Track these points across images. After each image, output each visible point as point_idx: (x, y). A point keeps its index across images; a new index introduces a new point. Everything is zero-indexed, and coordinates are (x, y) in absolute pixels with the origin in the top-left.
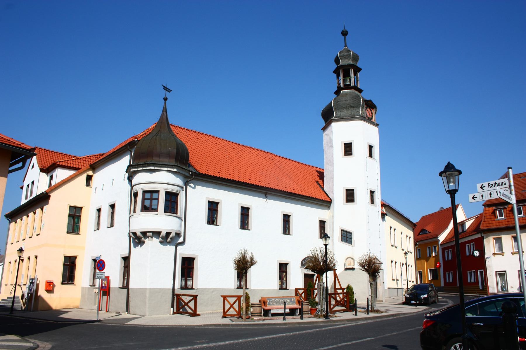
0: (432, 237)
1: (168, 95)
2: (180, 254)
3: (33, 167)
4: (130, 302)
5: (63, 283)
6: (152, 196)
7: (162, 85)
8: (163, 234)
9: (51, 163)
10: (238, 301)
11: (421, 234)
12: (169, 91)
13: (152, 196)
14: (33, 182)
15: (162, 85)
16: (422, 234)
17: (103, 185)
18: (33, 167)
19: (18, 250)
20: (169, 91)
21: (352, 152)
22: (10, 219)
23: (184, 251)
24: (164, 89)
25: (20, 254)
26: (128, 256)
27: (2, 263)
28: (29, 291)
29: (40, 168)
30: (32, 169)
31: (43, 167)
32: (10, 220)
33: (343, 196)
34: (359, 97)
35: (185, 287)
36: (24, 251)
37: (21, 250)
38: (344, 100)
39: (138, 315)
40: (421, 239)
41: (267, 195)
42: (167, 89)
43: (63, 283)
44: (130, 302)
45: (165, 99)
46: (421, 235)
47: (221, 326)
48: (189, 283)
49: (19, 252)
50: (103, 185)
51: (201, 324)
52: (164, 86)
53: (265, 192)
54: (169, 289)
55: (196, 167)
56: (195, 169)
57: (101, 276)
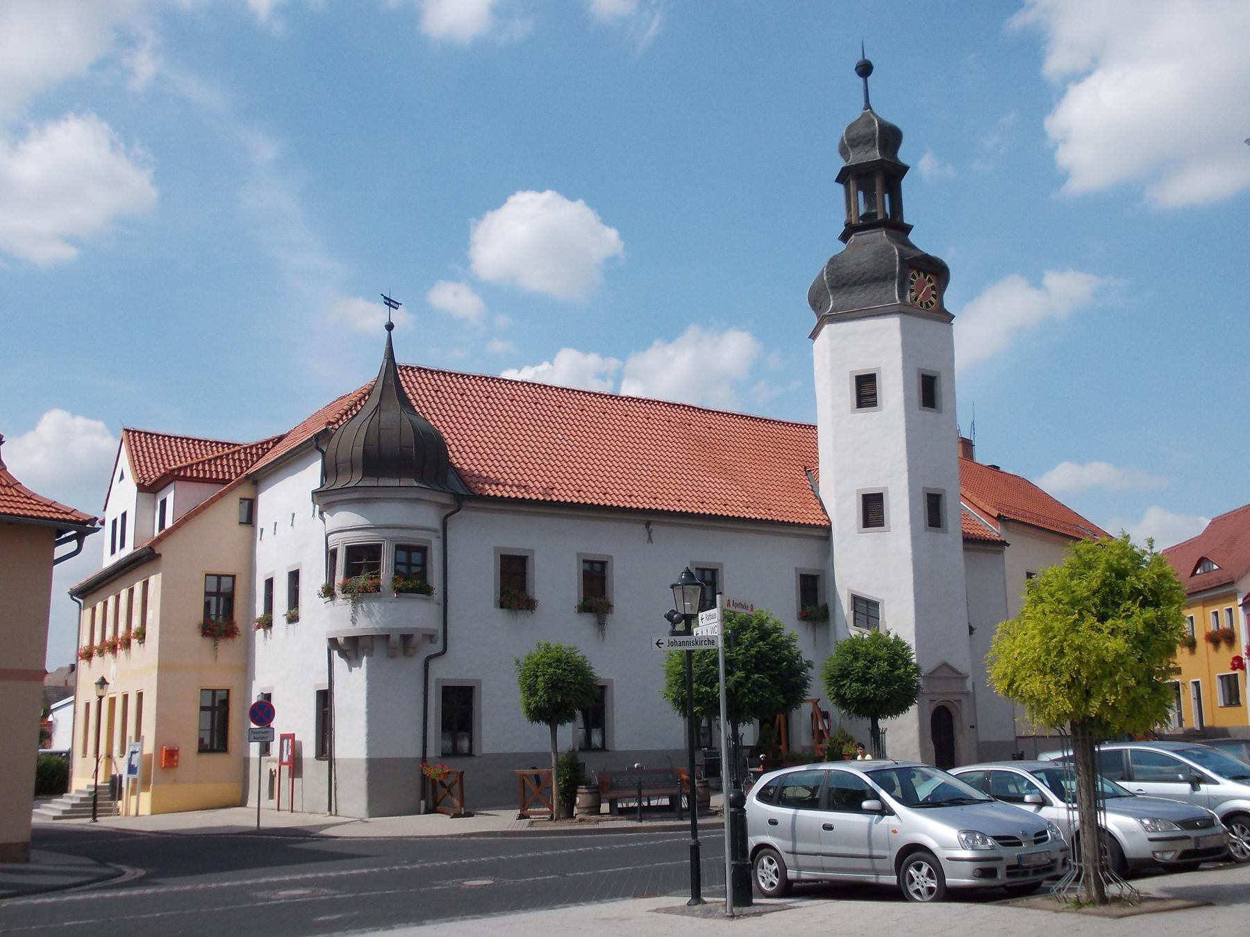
0: (1220, 582)
1: (398, 317)
2: (438, 681)
3: (122, 477)
4: (335, 789)
5: (203, 749)
6: (409, 557)
7: (382, 295)
8: (395, 638)
9: (158, 474)
10: (1117, 782)
11: (1198, 572)
12: (396, 306)
13: (409, 557)
14: (124, 515)
15: (382, 295)
16: (1202, 572)
17: (276, 524)
18: (122, 477)
19: (96, 683)
20: (396, 306)
21: (876, 394)
22: (82, 599)
23: (448, 671)
24: (386, 303)
25: (102, 690)
26: (327, 688)
27: (71, 698)
28: (825, 760)
29: (138, 483)
30: (121, 482)
31: (142, 481)
32: (81, 601)
33: (854, 510)
34: (892, 252)
35: (452, 753)
36: (108, 684)
37: (103, 683)
38: (854, 261)
39: (350, 817)
40: (1194, 589)
41: (651, 527)
42: (392, 303)
43: (203, 749)
44: (335, 789)
45: (390, 327)
46: (1199, 574)
47: (499, 836)
48: (464, 744)
49: (99, 685)
50: (276, 524)
51: (459, 833)
52: (385, 298)
53: (644, 521)
54: (356, 761)
55: (469, 479)
56: (466, 485)
57: (265, 735)
